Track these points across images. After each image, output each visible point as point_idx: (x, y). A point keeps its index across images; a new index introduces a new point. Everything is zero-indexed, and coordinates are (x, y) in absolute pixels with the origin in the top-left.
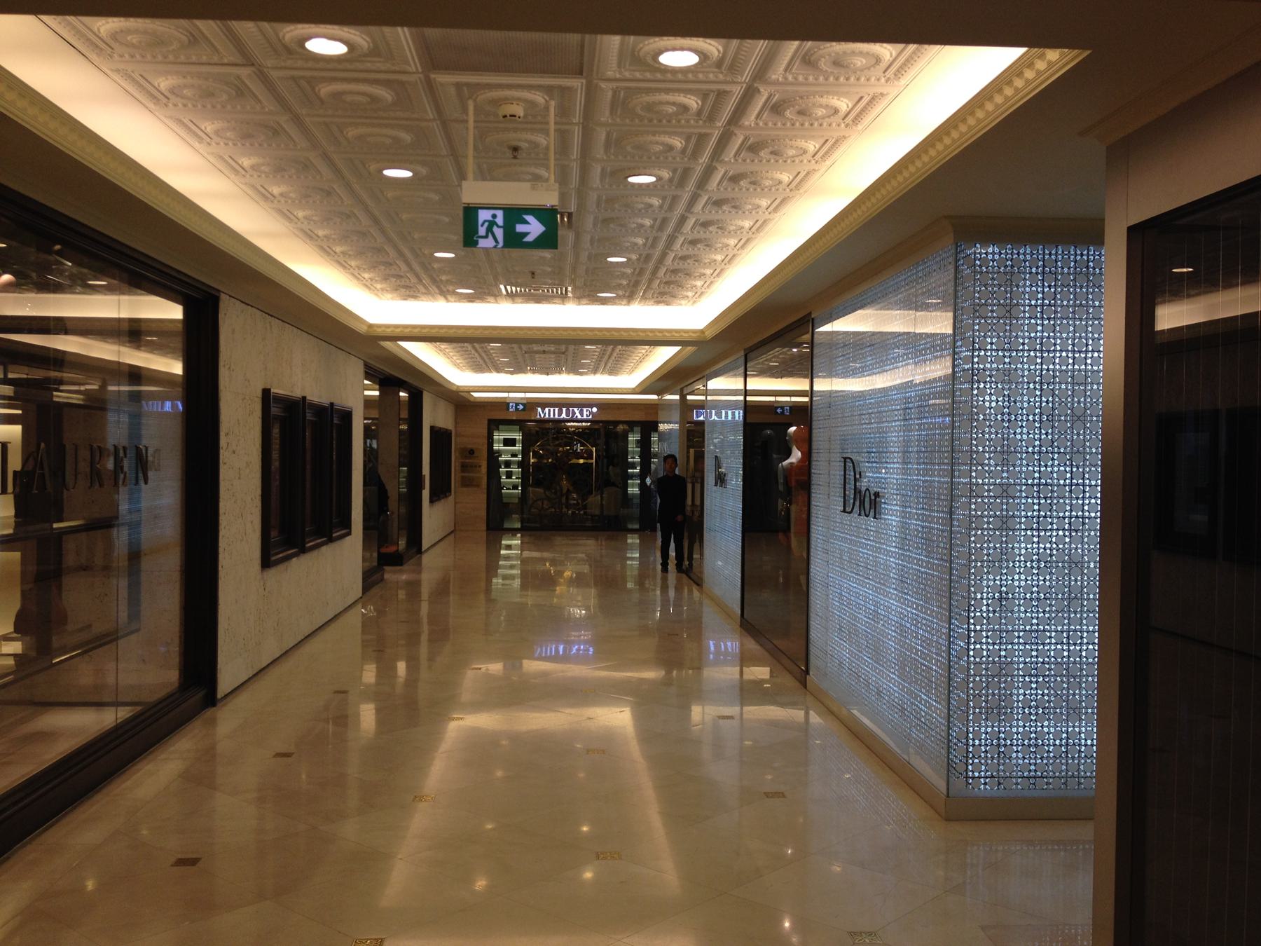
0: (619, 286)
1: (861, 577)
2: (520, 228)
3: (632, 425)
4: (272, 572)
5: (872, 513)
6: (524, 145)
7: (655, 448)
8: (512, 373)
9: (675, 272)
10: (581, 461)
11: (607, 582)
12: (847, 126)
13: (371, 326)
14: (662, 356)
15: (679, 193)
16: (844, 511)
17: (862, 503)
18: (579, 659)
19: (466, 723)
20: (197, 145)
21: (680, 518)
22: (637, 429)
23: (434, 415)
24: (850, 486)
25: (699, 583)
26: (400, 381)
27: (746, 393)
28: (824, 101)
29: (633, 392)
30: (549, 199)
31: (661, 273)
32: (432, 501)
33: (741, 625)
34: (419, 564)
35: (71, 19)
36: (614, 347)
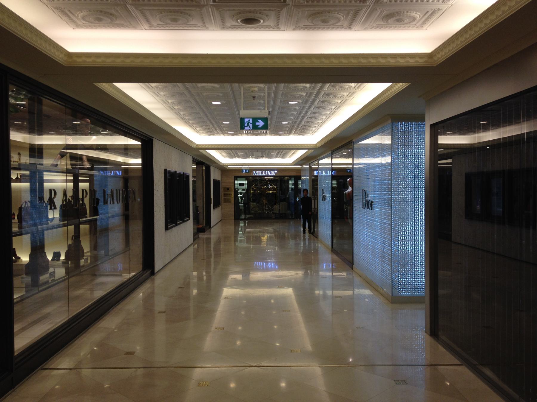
0: (286, 130)
1: (368, 229)
2: (257, 124)
3: (290, 177)
4: (168, 231)
6: (257, 96)
7: (300, 186)
8: (244, 158)
9: (305, 126)
10: (271, 192)
11: (281, 238)
13: (197, 145)
14: (301, 153)
15: (305, 105)
18: (271, 270)
19: (227, 292)
20: (156, 97)
21: (310, 213)
22: (293, 179)
23: (215, 175)
24: (364, 200)
25: (317, 237)
26: (204, 163)
27: (332, 164)
29: (291, 164)
30: (265, 114)
31: (300, 126)
32: (214, 208)
33: (332, 251)
34: (210, 232)
35: (147, 84)
36: (283, 150)
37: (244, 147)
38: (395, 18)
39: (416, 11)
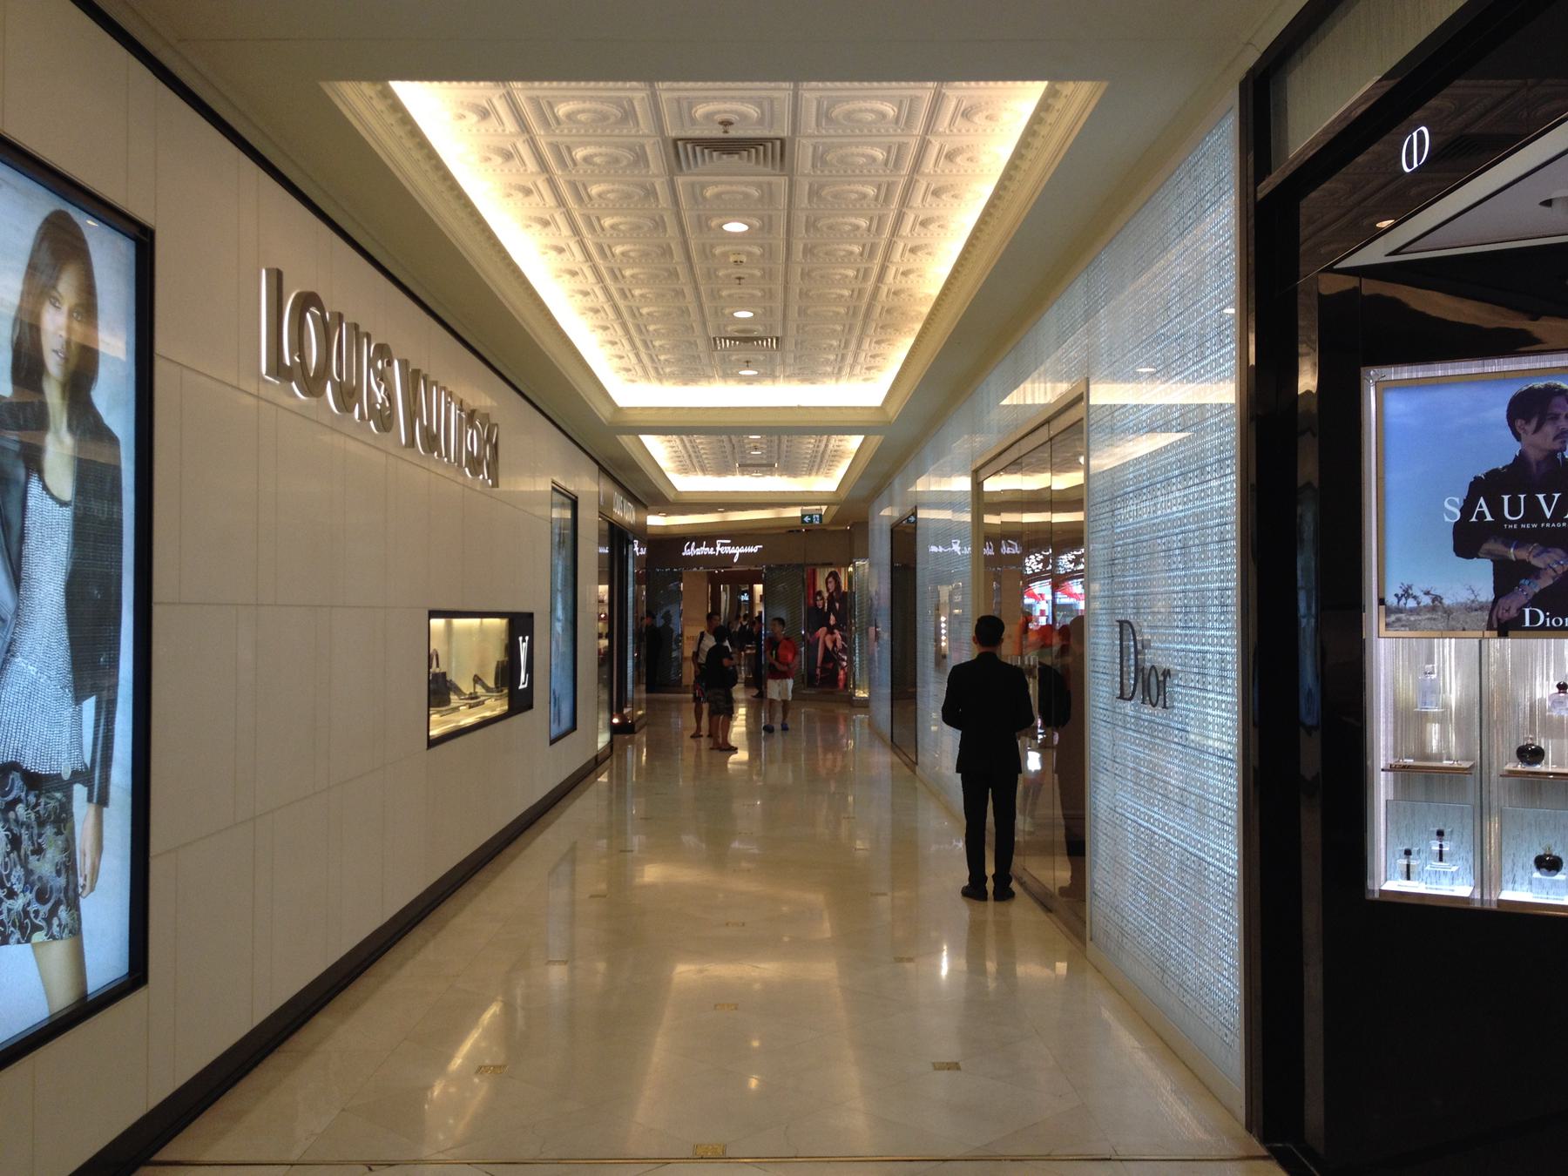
5: (1161, 702)
16: (1121, 697)
17: (1146, 689)
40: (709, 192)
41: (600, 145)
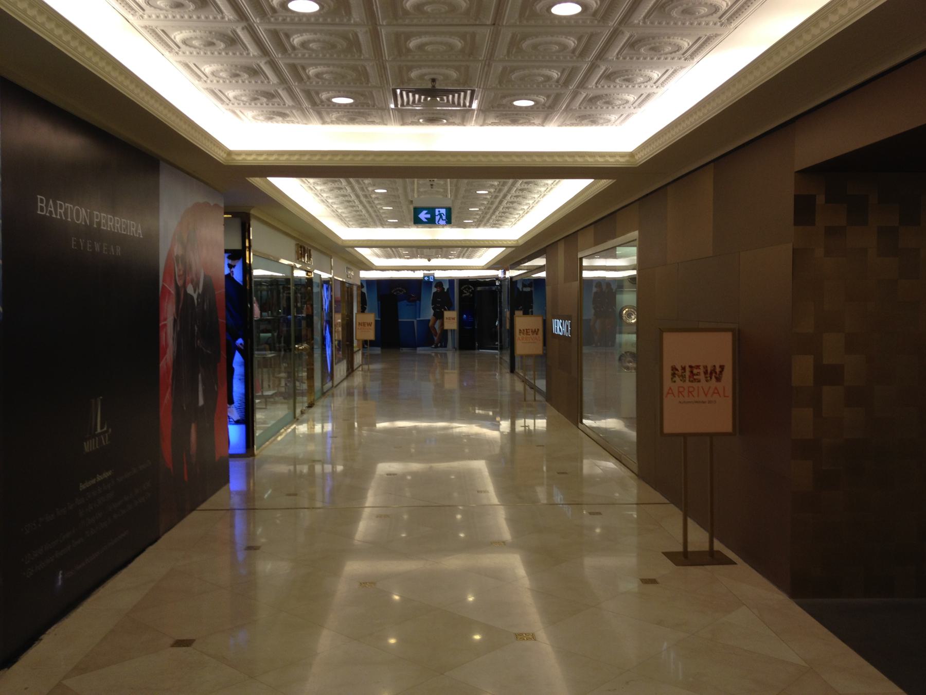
2: (429, 216)
12: (721, 25)
13: (230, 153)
28: (620, 96)
31: (497, 213)
36: (468, 248)
37: (391, 162)
38: (648, 47)
39: (682, 36)
40: (413, 44)
41: (328, 65)
